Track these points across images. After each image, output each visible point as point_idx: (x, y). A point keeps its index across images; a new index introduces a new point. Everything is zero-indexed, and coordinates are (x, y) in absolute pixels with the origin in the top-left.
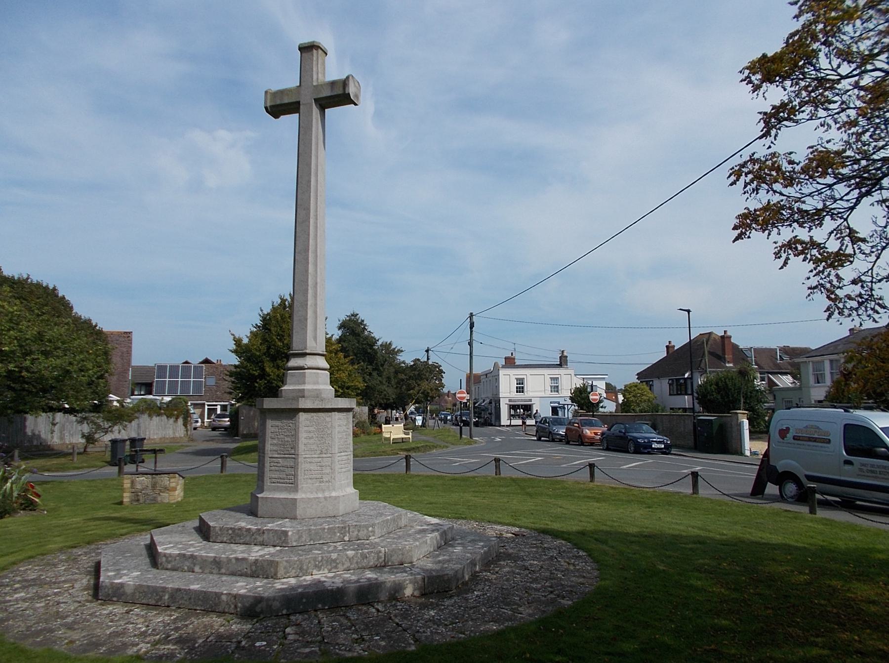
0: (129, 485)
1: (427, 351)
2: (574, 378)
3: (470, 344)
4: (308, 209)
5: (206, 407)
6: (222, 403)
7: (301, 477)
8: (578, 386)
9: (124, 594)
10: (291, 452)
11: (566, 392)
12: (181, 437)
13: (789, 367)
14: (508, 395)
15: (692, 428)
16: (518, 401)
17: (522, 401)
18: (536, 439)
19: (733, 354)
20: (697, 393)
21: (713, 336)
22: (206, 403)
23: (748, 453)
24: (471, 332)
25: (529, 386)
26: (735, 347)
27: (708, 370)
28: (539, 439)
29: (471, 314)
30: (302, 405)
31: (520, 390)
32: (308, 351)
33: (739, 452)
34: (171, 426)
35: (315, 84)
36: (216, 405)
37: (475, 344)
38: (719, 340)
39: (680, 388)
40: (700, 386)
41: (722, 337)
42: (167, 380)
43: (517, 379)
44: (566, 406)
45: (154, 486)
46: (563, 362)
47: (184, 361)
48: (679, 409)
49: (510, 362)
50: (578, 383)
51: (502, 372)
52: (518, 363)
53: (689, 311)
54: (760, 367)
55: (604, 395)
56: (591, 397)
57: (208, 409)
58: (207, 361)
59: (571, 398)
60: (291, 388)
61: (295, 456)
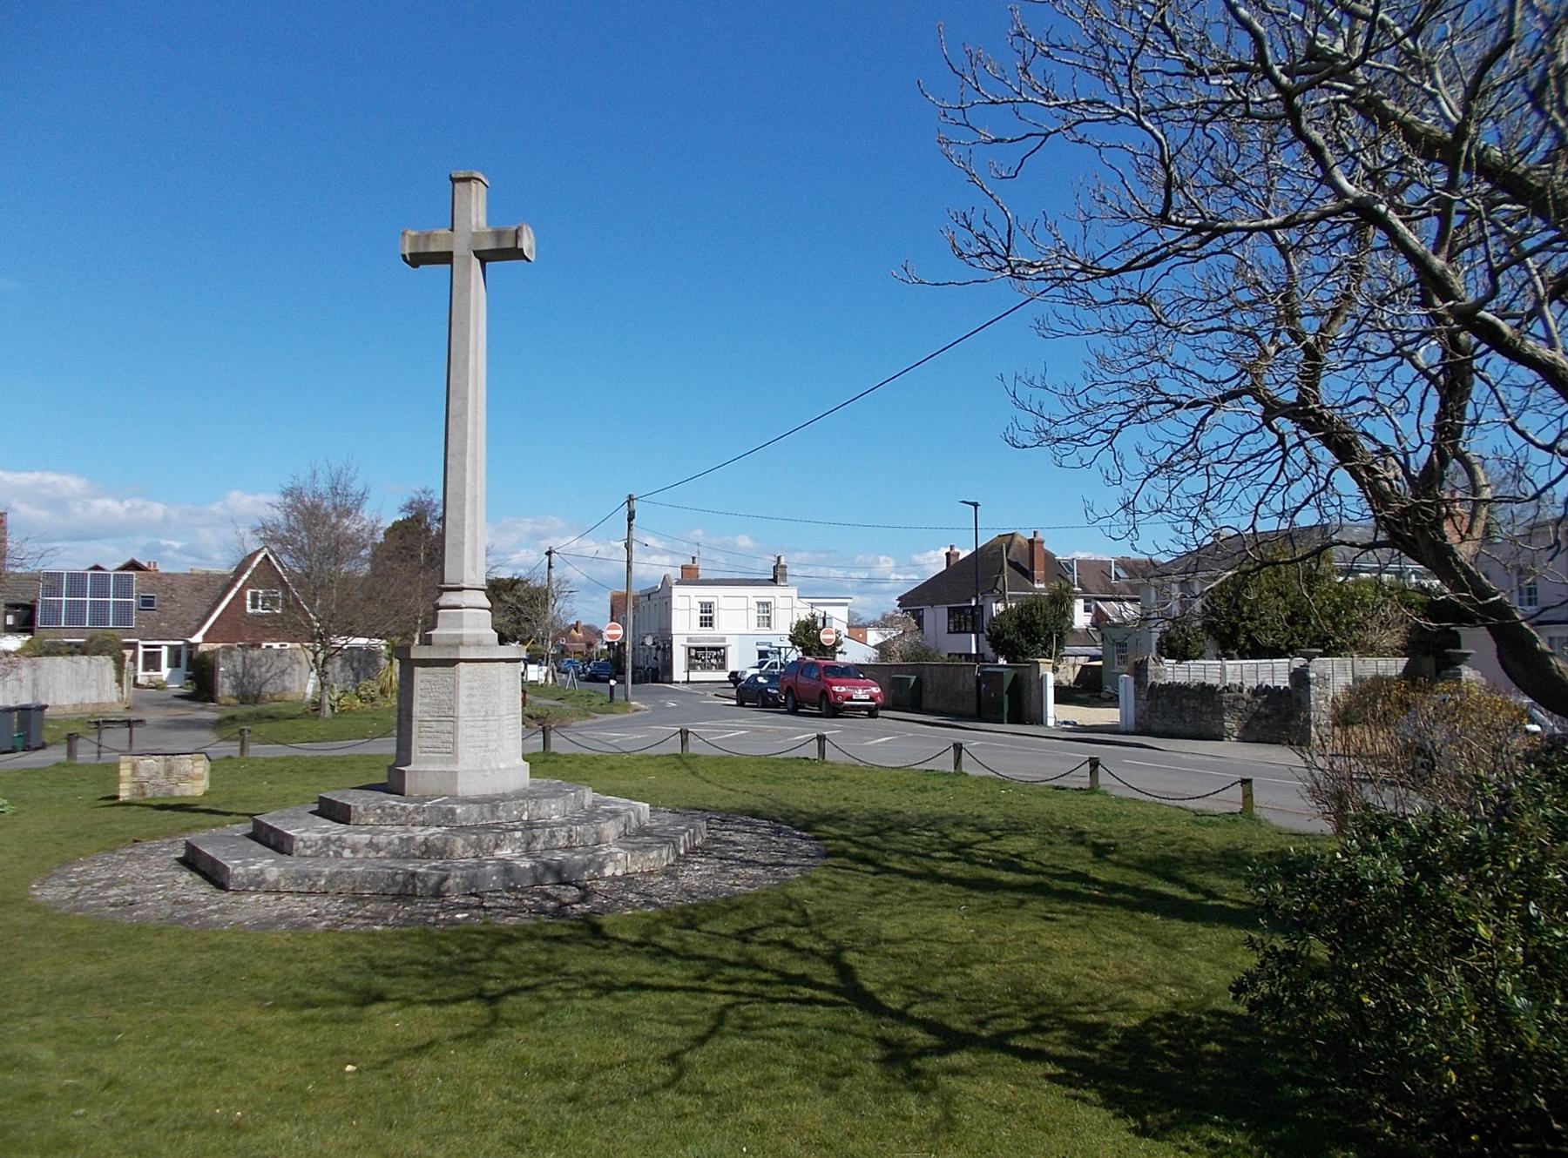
0: (128, 772)
1: (549, 553)
2: (798, 603)
3: (628, 546)
4: (466, 399)
5: (141, 650)
6: (172, 643)
7: (461, 745)
8: (803, 618)
9: (264, 881)
10: (448, 714)
11: (783, 625)
12: (112, 703)
13: (1128, 591)
14: (685, 629)
15: (974, 685)
16: (704, 640)
17: (710, 640)
18: (734, 703)
19: (1046, 568)
20: (989, 630)
21: (1018, 539)
22: (141, 643)
23: (1051, 722)
24: (630, 526)
25: (720, 618)
26: (1049, 557)
27: (1008, 593)
28: (741, 704)
29: (630, 496)
30: (464, 653)
31: (707, 622)
32: (465, 586)
33: (1040, 720)
34: (94, 684)
35: (474, 230)
36: (159, 647)
37: (634, 546)
38: (1026, 546)
39: (964, 620)
40: (994, 619)
41: (1031, 542)
42: (88, 599)
43: (702, 604)
44: (783, 650)
45: (169, 771)
46: (777, 577)
47: (92, 565)
48: (960, 655)
49: (690, 577)
50: (804, 615)
51: (677, 591)
52: (702, 575)
53: (976, 505)
54: (1085, 590)
55: (845, 631)
56: (823, 637)
57: (145, 654)
58: (134, 565)
59: (791, 638)
60: (444, 632)
61: (453, 719)
